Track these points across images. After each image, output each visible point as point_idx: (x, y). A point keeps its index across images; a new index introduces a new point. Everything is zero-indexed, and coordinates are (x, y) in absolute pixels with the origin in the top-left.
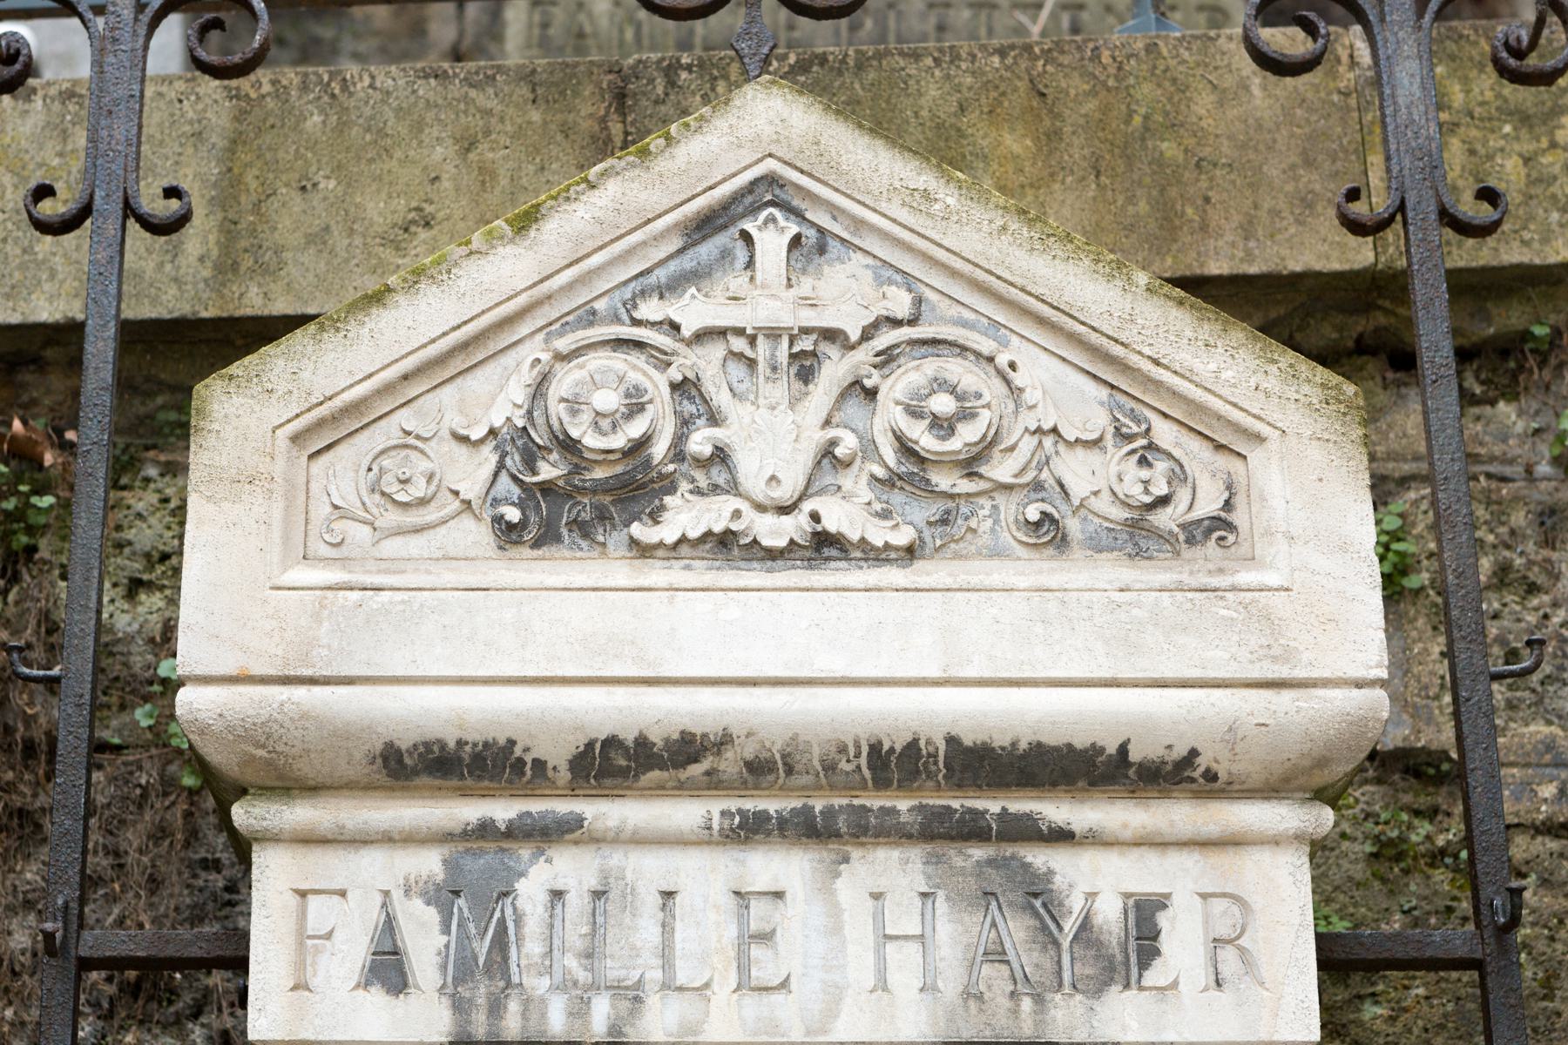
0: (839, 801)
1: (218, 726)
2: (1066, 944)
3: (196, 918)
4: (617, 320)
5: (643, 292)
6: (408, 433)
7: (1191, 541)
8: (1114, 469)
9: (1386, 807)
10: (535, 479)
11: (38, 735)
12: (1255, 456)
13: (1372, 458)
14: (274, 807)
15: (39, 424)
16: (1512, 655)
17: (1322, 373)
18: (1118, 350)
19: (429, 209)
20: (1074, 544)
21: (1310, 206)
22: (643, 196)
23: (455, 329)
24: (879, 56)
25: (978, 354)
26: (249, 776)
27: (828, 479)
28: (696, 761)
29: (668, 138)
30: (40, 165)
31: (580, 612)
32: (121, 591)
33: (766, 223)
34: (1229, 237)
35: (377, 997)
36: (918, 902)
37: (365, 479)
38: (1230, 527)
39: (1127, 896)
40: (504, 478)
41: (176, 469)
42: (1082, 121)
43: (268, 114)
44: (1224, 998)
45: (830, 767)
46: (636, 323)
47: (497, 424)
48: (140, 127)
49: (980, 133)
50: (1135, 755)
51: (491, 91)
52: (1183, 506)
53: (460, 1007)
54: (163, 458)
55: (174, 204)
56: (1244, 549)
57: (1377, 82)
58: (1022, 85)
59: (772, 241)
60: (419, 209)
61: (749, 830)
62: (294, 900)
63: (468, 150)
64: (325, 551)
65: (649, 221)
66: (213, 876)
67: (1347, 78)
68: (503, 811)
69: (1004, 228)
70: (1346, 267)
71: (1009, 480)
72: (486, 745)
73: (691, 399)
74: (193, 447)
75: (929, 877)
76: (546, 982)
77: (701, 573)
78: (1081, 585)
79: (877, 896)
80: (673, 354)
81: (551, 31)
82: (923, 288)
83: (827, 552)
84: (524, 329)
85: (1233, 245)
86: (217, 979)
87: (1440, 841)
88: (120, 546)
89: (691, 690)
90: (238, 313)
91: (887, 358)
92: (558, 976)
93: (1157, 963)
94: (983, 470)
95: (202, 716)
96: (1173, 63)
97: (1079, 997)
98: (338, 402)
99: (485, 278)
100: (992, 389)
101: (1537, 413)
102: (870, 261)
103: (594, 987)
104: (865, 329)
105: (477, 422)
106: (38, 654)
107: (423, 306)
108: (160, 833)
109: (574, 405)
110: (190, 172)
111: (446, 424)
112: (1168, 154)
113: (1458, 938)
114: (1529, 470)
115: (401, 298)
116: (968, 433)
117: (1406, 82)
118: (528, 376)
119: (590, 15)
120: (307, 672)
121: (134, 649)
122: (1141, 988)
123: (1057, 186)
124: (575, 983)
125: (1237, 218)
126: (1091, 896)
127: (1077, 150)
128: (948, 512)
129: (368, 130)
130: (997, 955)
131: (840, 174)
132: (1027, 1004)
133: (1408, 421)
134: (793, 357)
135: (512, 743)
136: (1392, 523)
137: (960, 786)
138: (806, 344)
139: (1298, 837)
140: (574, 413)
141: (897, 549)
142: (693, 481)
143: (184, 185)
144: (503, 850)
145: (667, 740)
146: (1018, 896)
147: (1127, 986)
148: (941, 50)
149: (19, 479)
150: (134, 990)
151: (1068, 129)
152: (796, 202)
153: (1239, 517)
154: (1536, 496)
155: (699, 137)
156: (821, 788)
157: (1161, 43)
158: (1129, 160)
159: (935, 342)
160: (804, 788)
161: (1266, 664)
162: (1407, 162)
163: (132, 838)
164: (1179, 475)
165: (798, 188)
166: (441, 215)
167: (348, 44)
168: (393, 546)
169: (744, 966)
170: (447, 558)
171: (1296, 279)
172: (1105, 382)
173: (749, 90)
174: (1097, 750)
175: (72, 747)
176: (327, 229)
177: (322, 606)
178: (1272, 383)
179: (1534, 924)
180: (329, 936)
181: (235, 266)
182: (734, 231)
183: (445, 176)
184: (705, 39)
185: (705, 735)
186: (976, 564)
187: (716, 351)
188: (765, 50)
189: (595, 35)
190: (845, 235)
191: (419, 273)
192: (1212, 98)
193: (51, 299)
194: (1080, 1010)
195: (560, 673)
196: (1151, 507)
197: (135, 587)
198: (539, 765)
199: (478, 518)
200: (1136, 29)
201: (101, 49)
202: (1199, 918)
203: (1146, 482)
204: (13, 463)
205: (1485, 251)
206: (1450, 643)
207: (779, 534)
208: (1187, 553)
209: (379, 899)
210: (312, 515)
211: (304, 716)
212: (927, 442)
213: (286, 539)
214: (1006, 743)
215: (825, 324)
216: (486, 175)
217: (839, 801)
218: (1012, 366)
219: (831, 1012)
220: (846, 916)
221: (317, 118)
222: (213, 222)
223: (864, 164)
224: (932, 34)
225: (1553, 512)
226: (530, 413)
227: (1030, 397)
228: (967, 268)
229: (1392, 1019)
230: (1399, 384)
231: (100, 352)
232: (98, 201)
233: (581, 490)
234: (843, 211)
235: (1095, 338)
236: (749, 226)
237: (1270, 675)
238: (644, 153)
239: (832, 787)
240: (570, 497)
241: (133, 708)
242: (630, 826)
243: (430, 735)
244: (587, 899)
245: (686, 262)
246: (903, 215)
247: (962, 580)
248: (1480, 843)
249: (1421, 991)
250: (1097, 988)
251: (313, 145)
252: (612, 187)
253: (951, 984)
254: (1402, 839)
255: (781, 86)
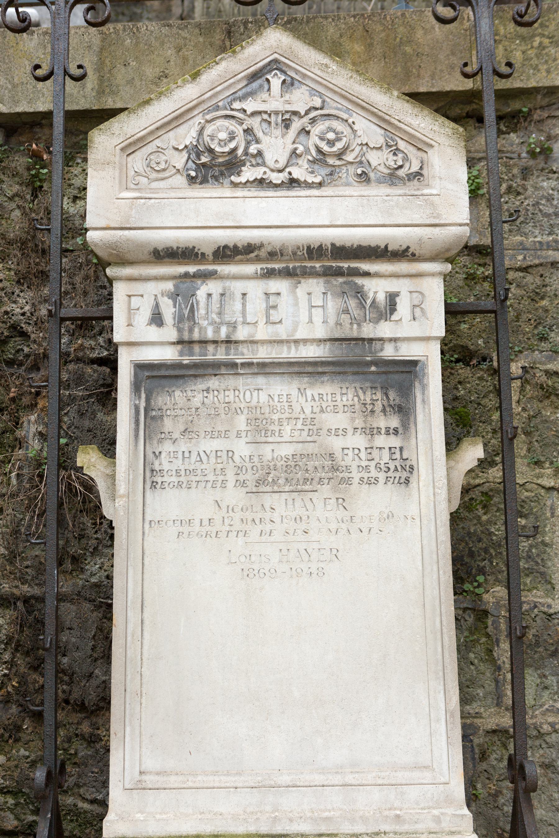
0: (297, 264)
1: (100, 244)
2: (367, 308)
3: (99, 304)
4: (226, 109)
5: (234, 99)
6: (159, 147)
7: (409, 180)
8: (385, 157)
9: (470, 263)
10: (200, 162)
11: (46, 247)
12: (430, 152)
13: (468, 151)
14: (119, 269)
15: (41, 145)
16: (511, 215)
17: (452, 124)
18: (387, 117)
19: (167, 72)
20: (372, 182)
21: (453, 68)
22: (234, 67)
23: (173, 112)
24: (314, 18)
25: (342, 119)
26: (111, 259)
27: (294, 161)
28: (252, 252)
29: (242, 47)
30: (37, 58)
31: (215, 205)
32: (71, 200)
33: (274, 75)
34: (427, 79)
35: (154, 328)
36: (322, 296)
37: (145, 163)
38: (422, 175)
39: (387, 292)
40: (190, 162)
41: (85, 160)
42: (380, 40)
43: (113, 39)
44: (416, 323)
45: (294, 254)
46: (232, 110)
47: (187, 144)
48: (68, 44)
49: (347, 44)
50: (390, 249)
51: (186, 31)
52: (407, 169)
53: (180, 330)
54: (82, 156)
55: (81, 70)
56: (426, 182)
57: (475, 26)
58: (361, 28)
59: (276, 82)
60: (163, 72)
61: (269, 274)
62: (127, 298)
63: (179, 51)
64: (133, 186)
65: (236, 75)
66: (104, 291)
67: (467, 25)
68: (192, 269)
69: (351, 77)
70: (464, 89)
71: (352, 160)
72: (186, 248)
73: (250, 135)
74: (89, 153)
75: (325, 288)
76: (206, 322)
77: (254, 192)
78: (374, 194)
79: (309, 294)
80: (244, 120)
81: (210, 10)
82: (325, 97)
83: (294, 185)
84: (196, 112)
85: (428, 82)
86: (106, 323)
87: (486, 274)
88: (70, 185)
89: (251, 230)
90: (105, 108)
91: (313, 121)
92: (210, 321)
93: (396, 313)
94: (344, 157)
95: (95, 240)
96: (410, 20)
97: (371, 324)
98: (135, 137)
99: (183, 95)
100: (347, 131)
101: (523, 136)
102: (308, 88)
103: (222, 323)
104: (306, 111)
105: (181, 143)
106: (45, 221)
107: (163, 105)
108: (86, 277)
109: (212, 137)
110: (87, 59)
111: (171, 144)
112: (408, 51)
113: (489, 304)
114: (519, 155)
115: (155, 102)
116: (339, 145)
117: (484, 26)
118: (197, 128)
119: (223, 4)
120: (128, 226)
121: (76, 219)
122: (390, 321)
123: (371, 62)
124: (216, 322)
125: (429, 73)
126: (376, 293)
127: (378, 50)
128: (332, 171)
129: (146, 44)
130: (346, 311)
131: (298, 59)
132: (355, 326)
133: (480, 141)
134: (283, 120)
135: (194, 247)
136: (475, 173)
137: (335, 259)
138: (287, 116)
139: (440, 273)
140: (212, 140)
141: (316, 183)
142: (251, 162)
143: (85, 65)
144: (192, 281)
145: (243, 246)
146: (353, 293)
147: (386, 320)
148: (334, 16)
149: (36, 164)
150: (81, 327)
151: (375, 43)
152: (284, 68)
153: (424, 172)
154: (521, 164)
155: (252, 46)
156: (291, 260)
157: (406, 13)
158: (395, 53)
159: (329, 115)
160: (286, 260)
161: (431, 219)
162: (483, 54)
163: (78, 279)
164: (406, 158)
165: (285, 63)
166: (171, 73)
167: (145, 15)
168: (155, 185)
169: (268, 316)
170: (172, 188)
171: (448, 93)
172: (383, 128)
173: (269, 30)
174: (378, 247)
175: (55, 250)
176: (133, 79)
177: (133, 205)
178: (436, 128)
179: (514, 299)
180: (138, 309)
181: (103, 92)
182: (264, 78)
183: (172, 60)
184: (261, 12)
185: (255, 244)
186: (341, 188)
187: (258, 119)
188: (275, 16)
189: (225, 11)
190: (300, 79)
191: (161, 93)
192: (422, 32)
193: (43, 103)
194: (371, 328)
195: (209, 225)
196: (397, 169)
197: (75, 199)
198: (203, 254)
199: (182, 175)
200: (399, 8)
201: (54, 16)
202: (409, 299)
203: (395, 161)
204: (34, 158)
205: (508, 83)
206: (490, 212)
207: (278, 179)
208: (408, 184)
209: (153, 297)
210: (129, 175)
211: (128, 240)
212: (326, 148)
213: (120, 182)
214: (350, 245)
215: (293, 109)
216: (185, 60)
217: (297, 264)
218: (353, 123)
219: (295, 330)
220: (300, 300)
221: (129, 41)
222: (95, 77)
223: (306, 55)
224: (336, 11)
225: (526, 169)
226: (198, 140)
227: (359, 133)
228: (339, 90)
229: (470, 329)
230: (480, 128)
231: (59, 121)
232: (55, 70)
233: (215, 166)
234: (299, 71)
235: (380, 113)
236: (269, 77)
237: (433, 223)
238: (234, 52)
239: (295, 260)
240: (211, 168)
241: (76, 238)
242: (232, 273)
243: (168, 245)
244: (219, 296)
245: (248, 89)
246: (319, 73)
247: (337, 193)
248: (497, 274)
249: (479, 320)
250: (376, 321)
251: (128, 50)
252: (224, 64)
253: (332, 321)
254: (475, 273)
255: (279, 29)
